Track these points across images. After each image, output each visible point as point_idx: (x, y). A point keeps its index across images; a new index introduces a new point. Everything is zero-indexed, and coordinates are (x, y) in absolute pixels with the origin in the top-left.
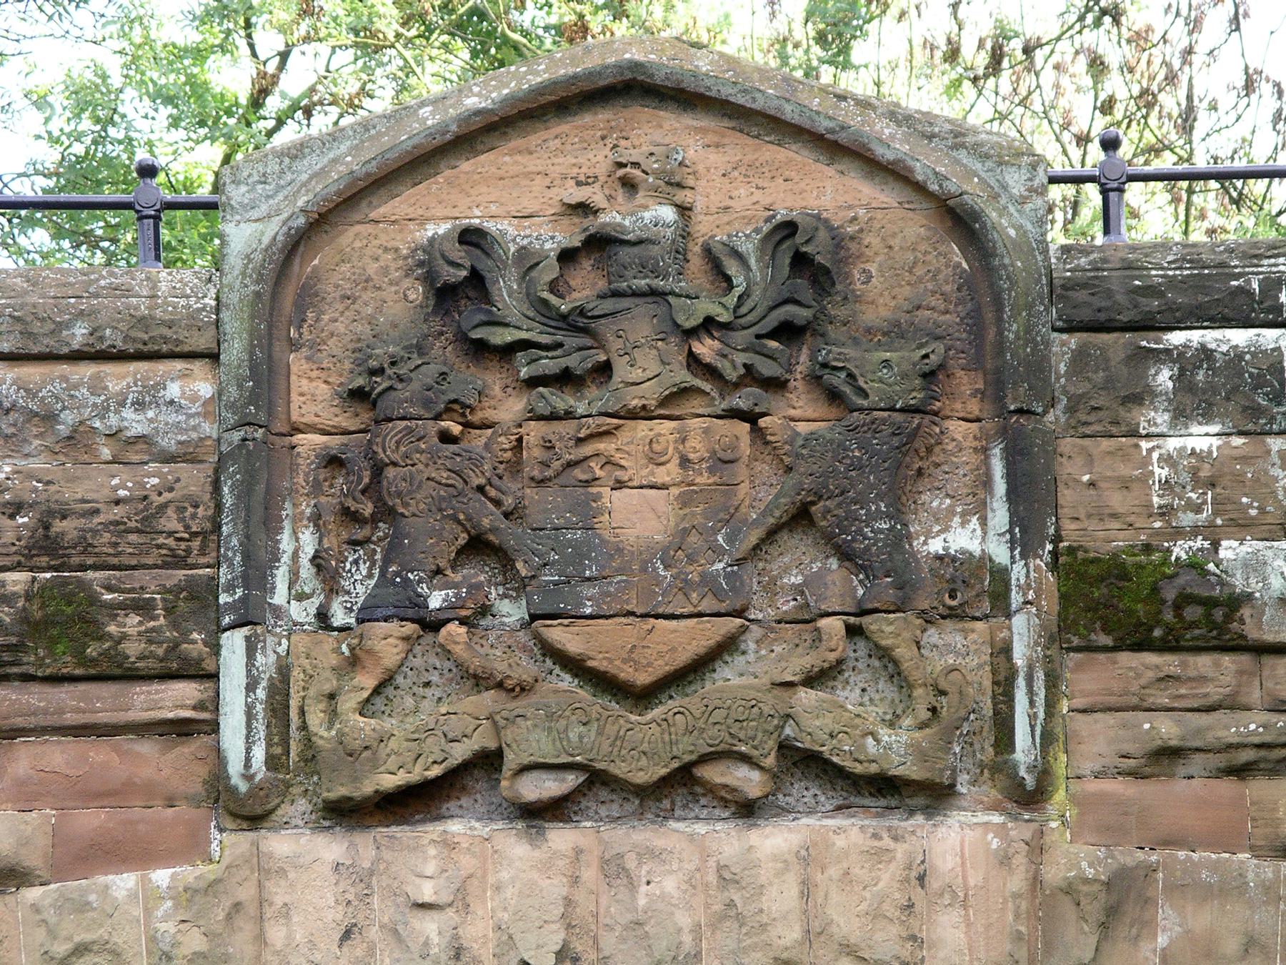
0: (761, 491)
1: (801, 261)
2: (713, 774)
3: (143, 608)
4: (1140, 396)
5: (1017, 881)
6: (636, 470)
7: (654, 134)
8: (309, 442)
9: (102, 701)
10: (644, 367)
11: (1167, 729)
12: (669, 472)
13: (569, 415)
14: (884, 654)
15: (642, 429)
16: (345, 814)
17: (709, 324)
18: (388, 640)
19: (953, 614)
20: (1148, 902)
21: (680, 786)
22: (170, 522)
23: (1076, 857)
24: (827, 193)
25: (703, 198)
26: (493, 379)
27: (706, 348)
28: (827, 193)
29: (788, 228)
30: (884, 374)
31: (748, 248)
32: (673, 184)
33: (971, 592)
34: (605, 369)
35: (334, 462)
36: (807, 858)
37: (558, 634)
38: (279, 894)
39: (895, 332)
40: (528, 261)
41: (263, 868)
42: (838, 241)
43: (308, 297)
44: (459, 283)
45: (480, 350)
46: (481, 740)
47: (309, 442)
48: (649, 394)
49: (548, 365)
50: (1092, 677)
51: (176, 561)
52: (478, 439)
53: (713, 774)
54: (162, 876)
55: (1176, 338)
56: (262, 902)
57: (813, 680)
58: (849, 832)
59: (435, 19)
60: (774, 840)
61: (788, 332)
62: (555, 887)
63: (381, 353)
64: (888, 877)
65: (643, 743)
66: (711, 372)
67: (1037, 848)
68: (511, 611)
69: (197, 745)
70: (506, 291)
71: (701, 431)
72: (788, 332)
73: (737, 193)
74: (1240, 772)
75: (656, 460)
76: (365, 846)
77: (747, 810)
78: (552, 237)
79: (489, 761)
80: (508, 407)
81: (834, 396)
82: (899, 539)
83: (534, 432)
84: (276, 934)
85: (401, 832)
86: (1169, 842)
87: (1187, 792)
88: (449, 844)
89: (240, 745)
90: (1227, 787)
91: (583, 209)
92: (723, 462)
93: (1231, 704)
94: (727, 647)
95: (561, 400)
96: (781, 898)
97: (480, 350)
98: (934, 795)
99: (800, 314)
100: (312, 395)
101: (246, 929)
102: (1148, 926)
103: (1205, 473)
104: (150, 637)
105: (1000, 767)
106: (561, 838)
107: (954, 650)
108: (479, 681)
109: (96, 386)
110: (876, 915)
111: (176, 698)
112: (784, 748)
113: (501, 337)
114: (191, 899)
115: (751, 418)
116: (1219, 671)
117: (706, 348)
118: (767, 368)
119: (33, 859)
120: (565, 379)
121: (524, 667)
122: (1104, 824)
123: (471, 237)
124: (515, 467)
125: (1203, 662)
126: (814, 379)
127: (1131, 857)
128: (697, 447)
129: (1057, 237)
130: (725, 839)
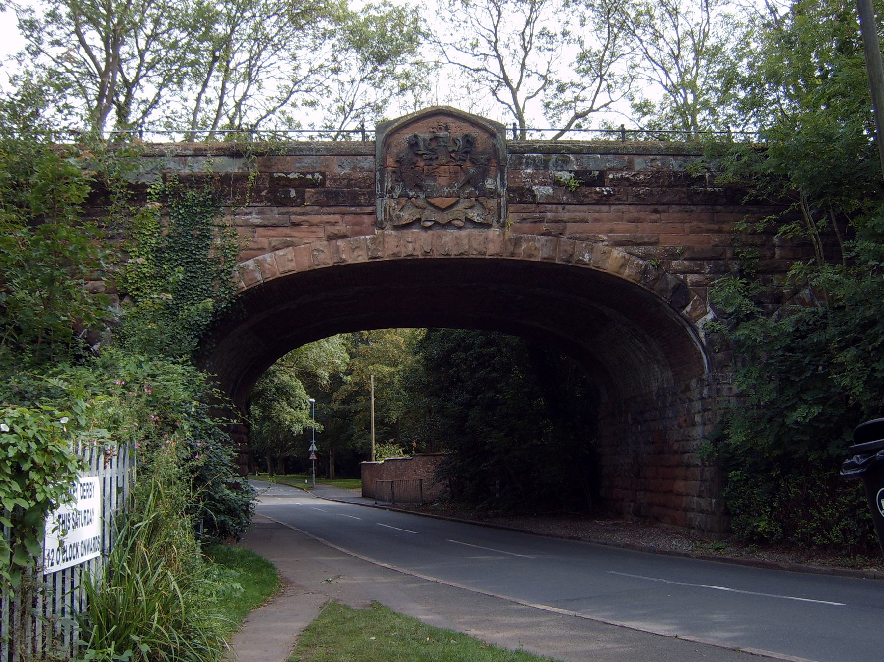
0: (462, 178)
1: (468, 141)
2: (456, 222)
3: (364, 195)
4: (521, 164)
6: (442, 174)
7: (443, 120)
9: (358, 210)
10: (443, 159)
11: (524, 216)
12: (448, 174)
14: (481, 204)
16: (397, 228)
17: (454, 151)
18: (403, 201)
21: (449, 225)
23: (509, 234)
25: (452, 130)
26: (419, 159)
27: (453, 155)
29: (466, 136)
30: (482, 158)
32: (447, 128)
33: (493, 194)
34: (437, 158)
35: (394, 172)
36: (469, 235)
37: (430, 200)
38: (387, 239)
39: (482, 153)
40: (424, 140)
41: (383, 235)
42: (473, 138)
43: (389, 146)
44: (414, 144)
45: (417, 154)
46: (418, 216)
49: (428, 157)
50: (512, 208)
51: (369, 187)
52: (417, 169)
53: (456, 222)
54: (368, 237)
56: (384, 241)
57: (470, 208)
58: (476, 231)
60: (463, 233)
61: (466, 152)
63: (401, 155)
64: (482, 238)
65: (444, 218)
66: (454, 158)
67: (504, 234)
68: (422, 196)
69: (372, 217)
70: (421, 144)
71: (452, 167)
72: (466, 152)
73: (458, 130)
74: (535, 222)
76: (399, 233)
77: (460, 228)
78: (428, 136)
80: (422, 164)
81: (473, 163)
82: (484, 185)
83: (426, 167)
84: (386, 246)
85: (405, 231)
87: (527, 226)
88: (412, 232)
89: (381, 216)
90: (533, 225)
91: (433, 132)
92: (456, 173)
93: (534, 212)
94: (457, 202)
95: (431, 162)
96: (465, 242)
97: (417, 154)
98: (488, 226)
100: (390, 161)
103: (531, 176)
105: (498, 222)
106: (430, 232)
107: (492, 203)
108: (417, 207)
110: (480, 244)
111: (369, 209)
112: (466, 218)
113: (420, 152)
114: (373, 240)
115: (460, 166)
116: (533, 207)
117: (453, 155)
119: (348, 234)
120: (431, 159)
121: (425, 205)
123: (416, 136)
124: (423, 173)
126: (470, 160)
128: (452, 171)
129: (202, 376)
130: (456, 232)
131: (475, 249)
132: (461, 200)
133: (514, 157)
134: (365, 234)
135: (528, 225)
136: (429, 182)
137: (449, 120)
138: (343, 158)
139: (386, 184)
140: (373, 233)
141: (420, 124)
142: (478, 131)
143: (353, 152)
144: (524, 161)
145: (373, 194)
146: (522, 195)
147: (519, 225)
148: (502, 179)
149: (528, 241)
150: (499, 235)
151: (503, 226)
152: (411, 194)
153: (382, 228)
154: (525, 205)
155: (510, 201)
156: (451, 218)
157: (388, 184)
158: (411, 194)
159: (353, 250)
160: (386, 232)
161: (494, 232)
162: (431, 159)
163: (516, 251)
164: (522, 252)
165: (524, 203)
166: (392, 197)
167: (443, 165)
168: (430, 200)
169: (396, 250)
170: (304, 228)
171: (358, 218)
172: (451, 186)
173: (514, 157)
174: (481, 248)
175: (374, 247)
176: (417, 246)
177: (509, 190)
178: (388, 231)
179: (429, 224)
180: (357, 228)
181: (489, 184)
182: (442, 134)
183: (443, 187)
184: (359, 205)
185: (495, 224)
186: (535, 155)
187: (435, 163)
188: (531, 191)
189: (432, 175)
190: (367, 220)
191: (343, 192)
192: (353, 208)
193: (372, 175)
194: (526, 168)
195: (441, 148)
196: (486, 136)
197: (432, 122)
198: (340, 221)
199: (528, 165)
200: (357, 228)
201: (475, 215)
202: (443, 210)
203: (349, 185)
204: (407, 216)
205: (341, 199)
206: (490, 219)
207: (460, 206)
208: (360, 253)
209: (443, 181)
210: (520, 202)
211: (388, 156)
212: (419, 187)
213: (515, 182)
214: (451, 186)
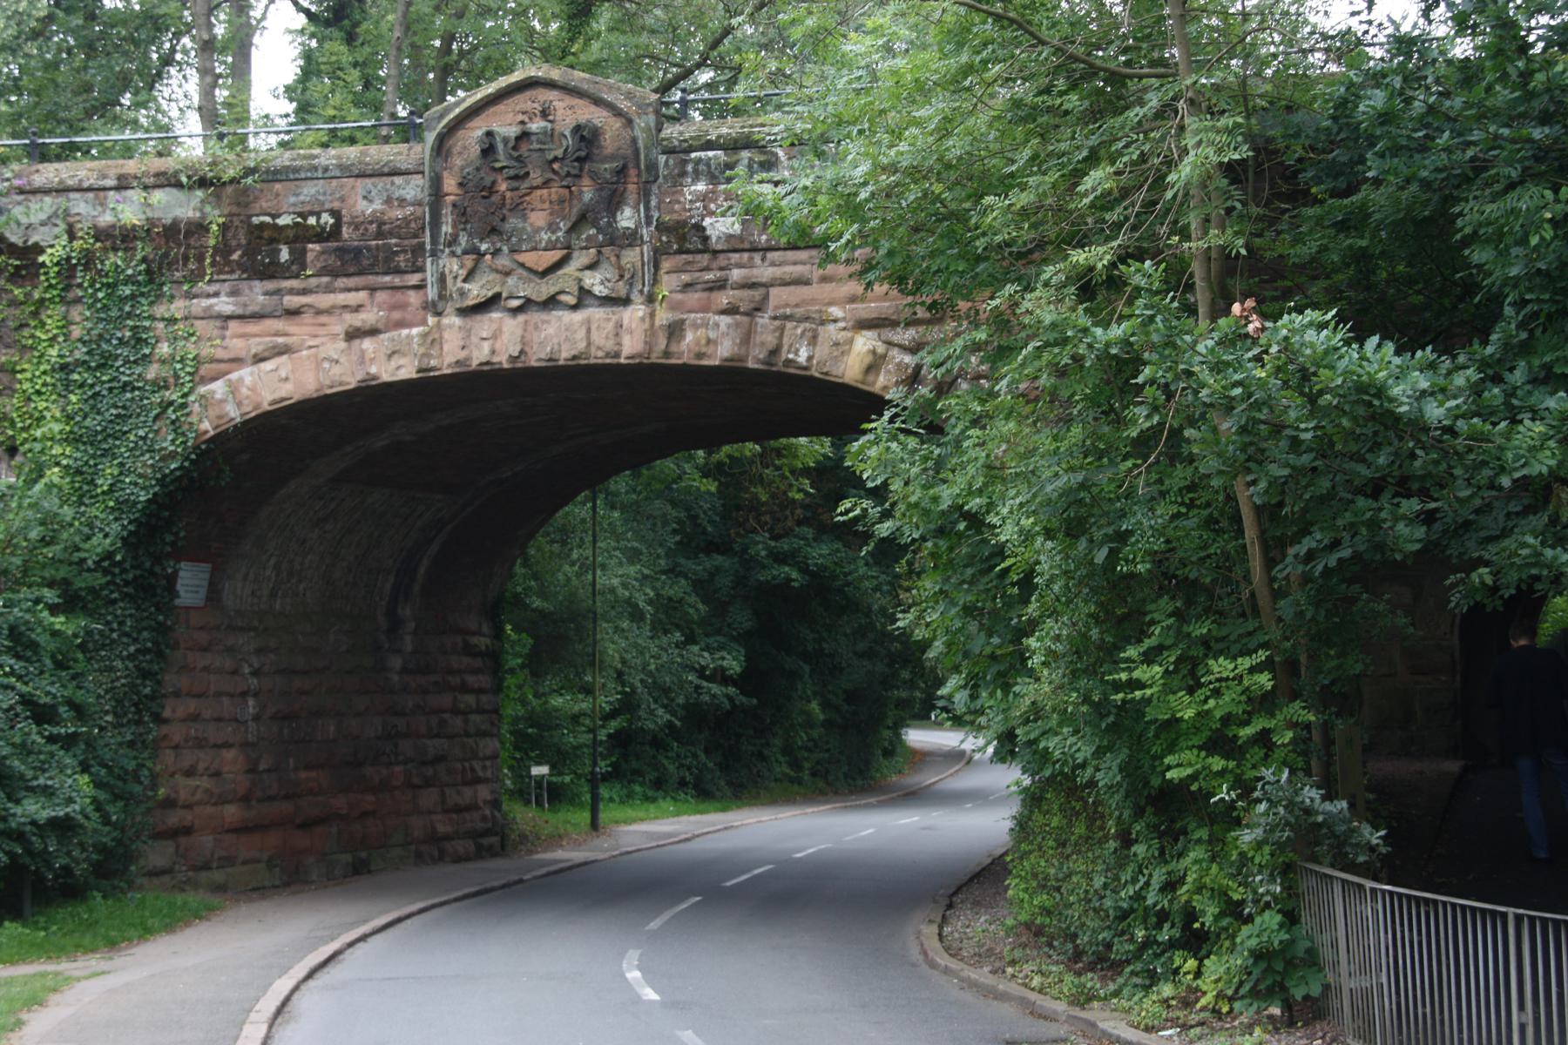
1: (582, 138)
2: (563, 298)
3: (405, 251)
4: (683, 174)
5: (647, 325)
8: (450, 199)
10: (536, 177)
12: (547, 205)
13: (517, 189)
15: (539, 192)
17: (556, 159)
18: (469, 261)
19: (630, 245)
20: (683, 330)
21: (551, 303)
22: (413, 225)
23: (663, 316)
24: (597, 116)
28: (597, 116)
31: (567, 133)
33: (632, 238)
34: (527, 174)
36: (588, 323)
38: (446, 335)
39: (612, 158)
40: (506, 140)
41: (438, 325)
43: (449, 154)
44: (488, 151)
45: (494, 169)
47: (450, 199)
48: (539, 181)
49: (512, 172)
51: (415, 236)
53: (563, 298)
54: (415, 331)
55: (693, 155)
58: (596, 313)
59: (1551, 257)
60: (578, 316)
62: (519, 332)
64: (611, 325)
65: (544, 289)
67: (652, 315)
69: (421, 292)
70: (500, 146)
74: (711, 289)
75: (543, 202)
77: (575, 308)
78: (513, 131)
79: (497, 296)
83: (508, 194)
84: (446, 347)
85: (479, 317)
86: (690, 312)
87: (694, 297)
88: (491, 320)
89: (432, 293)
90: (705, 295)
91: (522, 122)
92: (561, 201)
93: (707, 269)
95: (515, 184)
96: (581, 334)
98: (626, 301)
99: (583, 154)
100: (450, 184)
101: (437, 347)
102: (682, 337)
103: (704, 198)
104: (406, 260)
105: (641, 292)
106: (521, 318)
107: (631, 257)
109: (393, 183)
111: (414, 279)
112: (581, 289)
113: (498, 165)
115: (568, 187)
117: (556, 166)
118: (574, 172)
119: (380, 326)
120: (516, 177)
122: (674, 307)
125: (699, 257)
127: (679, 316)
128: (554, 197)
131: (599, 348)
132: (576, 254)
133: (671, 162)
134: (410, 325)
135: (697, 295)
136: (513, 222)
137: (552, 95)
138: (368, 181)
139: (444, 229)
140: (424, 322)
141: (501, 107)
142: (605, 113)
143: (386, 170)
144: (690, 168)
145: (422, 246)
146: (682, 239)
147: (679, 296)
148: (647, 209)
149: (695, 326)
150: (643, 319)
151: (650, 299)
152: (484, 247)
153: (439, 314)
154: (690, 257)
155: (658, 254)
156: (553, 290)
157: (447, 229)
158: (484, 247)
159: (390, 356)
160: (445, 321)
161: (635, 314)
162: (516, 177)
163: (674, 348)
164: (687, 348)
165: (688, 252)
166: (453, 254)
167: (537, 188)
168: (521, 258)
169: (462, 355)
170: (307, 318)
171: (399, 296)
172: (552, 227)
173: (671, 162)
174: (610, 345)
175: (422, 350)
176: (498, 346)
177: (661, 228)
178: (452, 320)
179: (515, 303)
180: (396, 315)
181: (626, 219)
182: (536, 126)
183: (538, 230)
184: (398, 271)
185: (635, 296)
186: (711, 154)
187: (526, 184)
188: (699, 228)
189: (519, 208)
190: (413, 298)
191: (369, 249)
192: (387, 279)
193: (419, 210)
194: (694, 182)
195: (536, 155)
196: (617, 124)
197: (523, 101)
198: (367, 302)
199: (697, 177)
200: (396, 315)
201: (596, 282)
202: (545, 273)
203: (380, 235)
204: (476, 291)
205: (366, 262)
206: (622, 288)
207: (570, 269)
208: (402, 361)
209: (538, 218)
210: (680, 252)
211: (445, 174)
212: (494, 231)
213: (673, 211)
214: (552, 227)
